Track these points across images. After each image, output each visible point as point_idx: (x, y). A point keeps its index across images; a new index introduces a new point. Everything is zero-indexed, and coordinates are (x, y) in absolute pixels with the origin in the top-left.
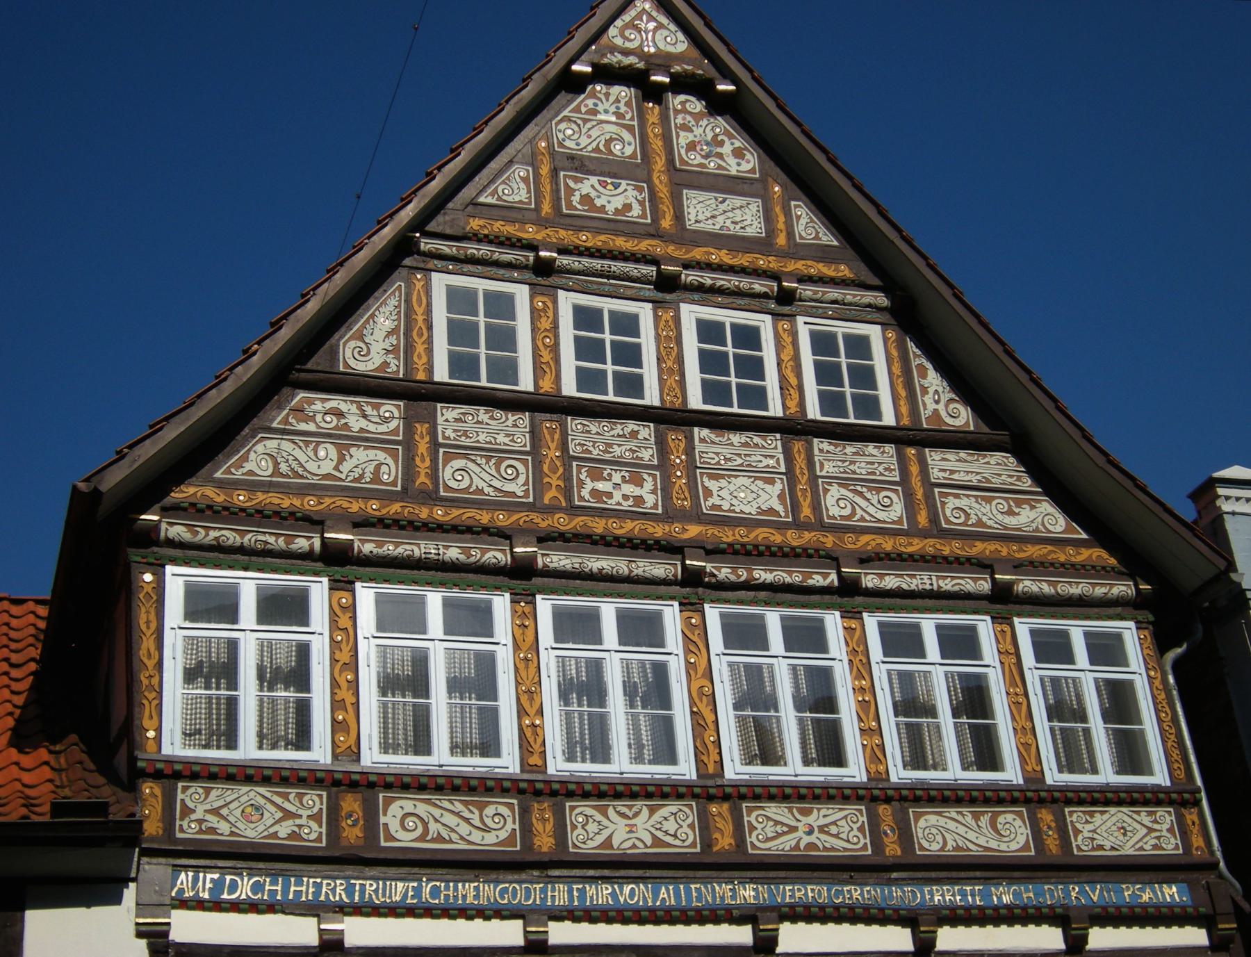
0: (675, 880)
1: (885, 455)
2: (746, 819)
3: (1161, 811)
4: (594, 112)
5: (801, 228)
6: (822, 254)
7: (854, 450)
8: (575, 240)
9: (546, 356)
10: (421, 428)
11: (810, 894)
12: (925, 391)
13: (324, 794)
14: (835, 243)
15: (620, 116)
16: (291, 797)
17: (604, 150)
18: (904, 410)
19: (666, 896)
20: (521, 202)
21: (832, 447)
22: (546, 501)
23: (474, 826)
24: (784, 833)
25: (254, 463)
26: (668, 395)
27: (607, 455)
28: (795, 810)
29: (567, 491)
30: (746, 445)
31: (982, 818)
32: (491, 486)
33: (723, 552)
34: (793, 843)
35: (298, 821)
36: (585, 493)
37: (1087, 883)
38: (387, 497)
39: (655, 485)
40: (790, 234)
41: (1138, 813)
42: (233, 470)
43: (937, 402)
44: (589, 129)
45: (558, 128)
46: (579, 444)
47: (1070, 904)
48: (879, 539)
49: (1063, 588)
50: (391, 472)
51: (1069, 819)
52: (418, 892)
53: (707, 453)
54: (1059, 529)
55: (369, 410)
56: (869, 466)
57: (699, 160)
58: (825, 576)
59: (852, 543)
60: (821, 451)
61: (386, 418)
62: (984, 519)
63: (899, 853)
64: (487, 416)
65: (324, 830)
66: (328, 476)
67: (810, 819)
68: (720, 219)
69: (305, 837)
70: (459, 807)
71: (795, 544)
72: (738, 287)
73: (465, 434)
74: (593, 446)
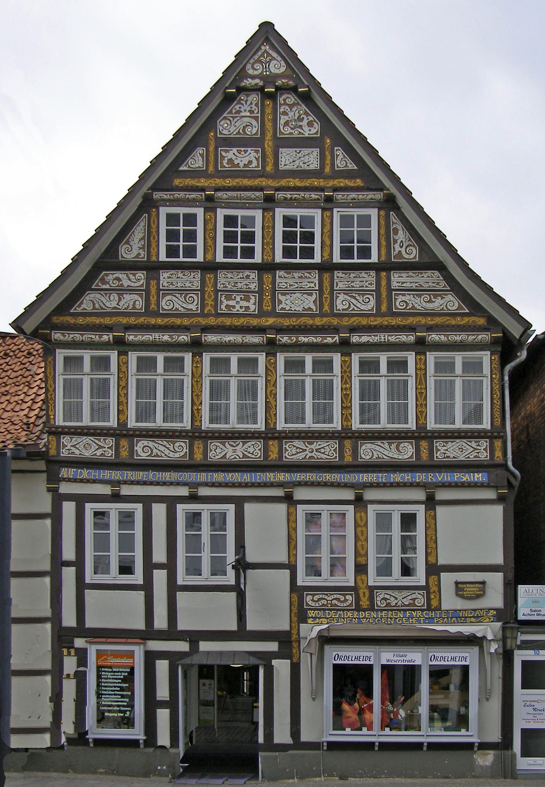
0: (248, 471)
1: (370, 277)
2: (284, 446)
3: (482, 441)
4: (239, 112)
5: (338, 161)
6: (348, 174)
7: (355, 275)
8: (224, 184)
9: (210, 242)
10: (153, 283)
11: (308, 477)
12: (395, 241)
13: (114, 439)
14: (356, 168)
15: (251, 112)
16: (102, 440)
17: (242, 133)
18: (383, 252)
19: (246, 478)
20: (199, 167)
21: (344, 275)
22: (206, 312)
23: (170, 450)
24: (300, 452)
25: (85, 305)
26: (266, 255)
27: (235, 288)
28: (306, 443)
29: (216, 307)
30: (301, 277)
31: (392, 445)
32: (182, 307)
33: (285, 330)
34: (304, 456)
35: (104, 449)
36: (223, 307)
37: (437, 472)
38: (138, 315)
39: (256, 301)
40: (333, 165)
41: (471, 442)
42: (77, 308)
43: (401, 247)
44: (236, 122)
45: (220, 124)
46: (222, 284)
47: (428, 482)
48: (360, 319)
49: (452, 337)
50: (140, 304)
51: (435, 445)
52: (148, 476)
53: (281, 283)
54: (454, 308)
55: (131, 277)
56: (361, 283)
57: (290, 131)
58: (333, 338)
59: (345, 322)
60: (338, 277)
61: (139, 279)
62: (416, 306)
63: (351, 460)
64: (182, 274)
65: (114, 453)
66: (115, 308)
67: (312, 446)
68: (297, 162)
69: (107, 455)
70: (165, 443)
71: (319, 324)
72: (304, 197)
73: (172, 284)
74: (229, 284)
